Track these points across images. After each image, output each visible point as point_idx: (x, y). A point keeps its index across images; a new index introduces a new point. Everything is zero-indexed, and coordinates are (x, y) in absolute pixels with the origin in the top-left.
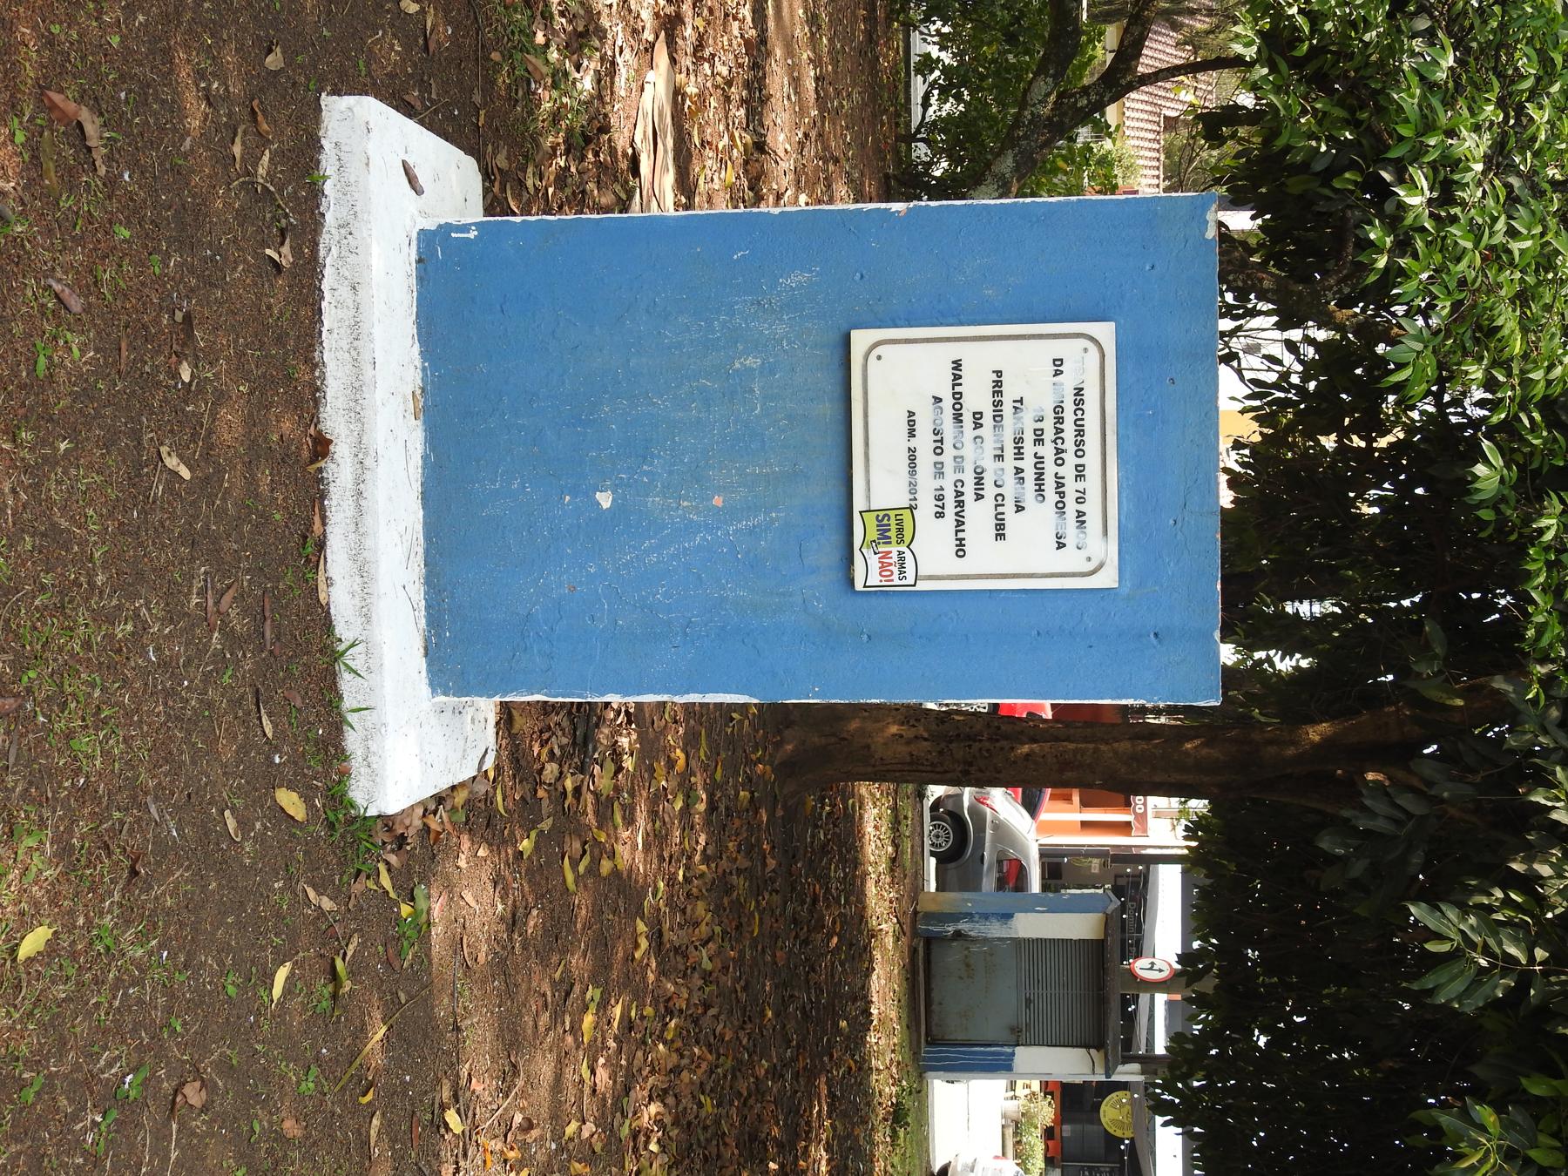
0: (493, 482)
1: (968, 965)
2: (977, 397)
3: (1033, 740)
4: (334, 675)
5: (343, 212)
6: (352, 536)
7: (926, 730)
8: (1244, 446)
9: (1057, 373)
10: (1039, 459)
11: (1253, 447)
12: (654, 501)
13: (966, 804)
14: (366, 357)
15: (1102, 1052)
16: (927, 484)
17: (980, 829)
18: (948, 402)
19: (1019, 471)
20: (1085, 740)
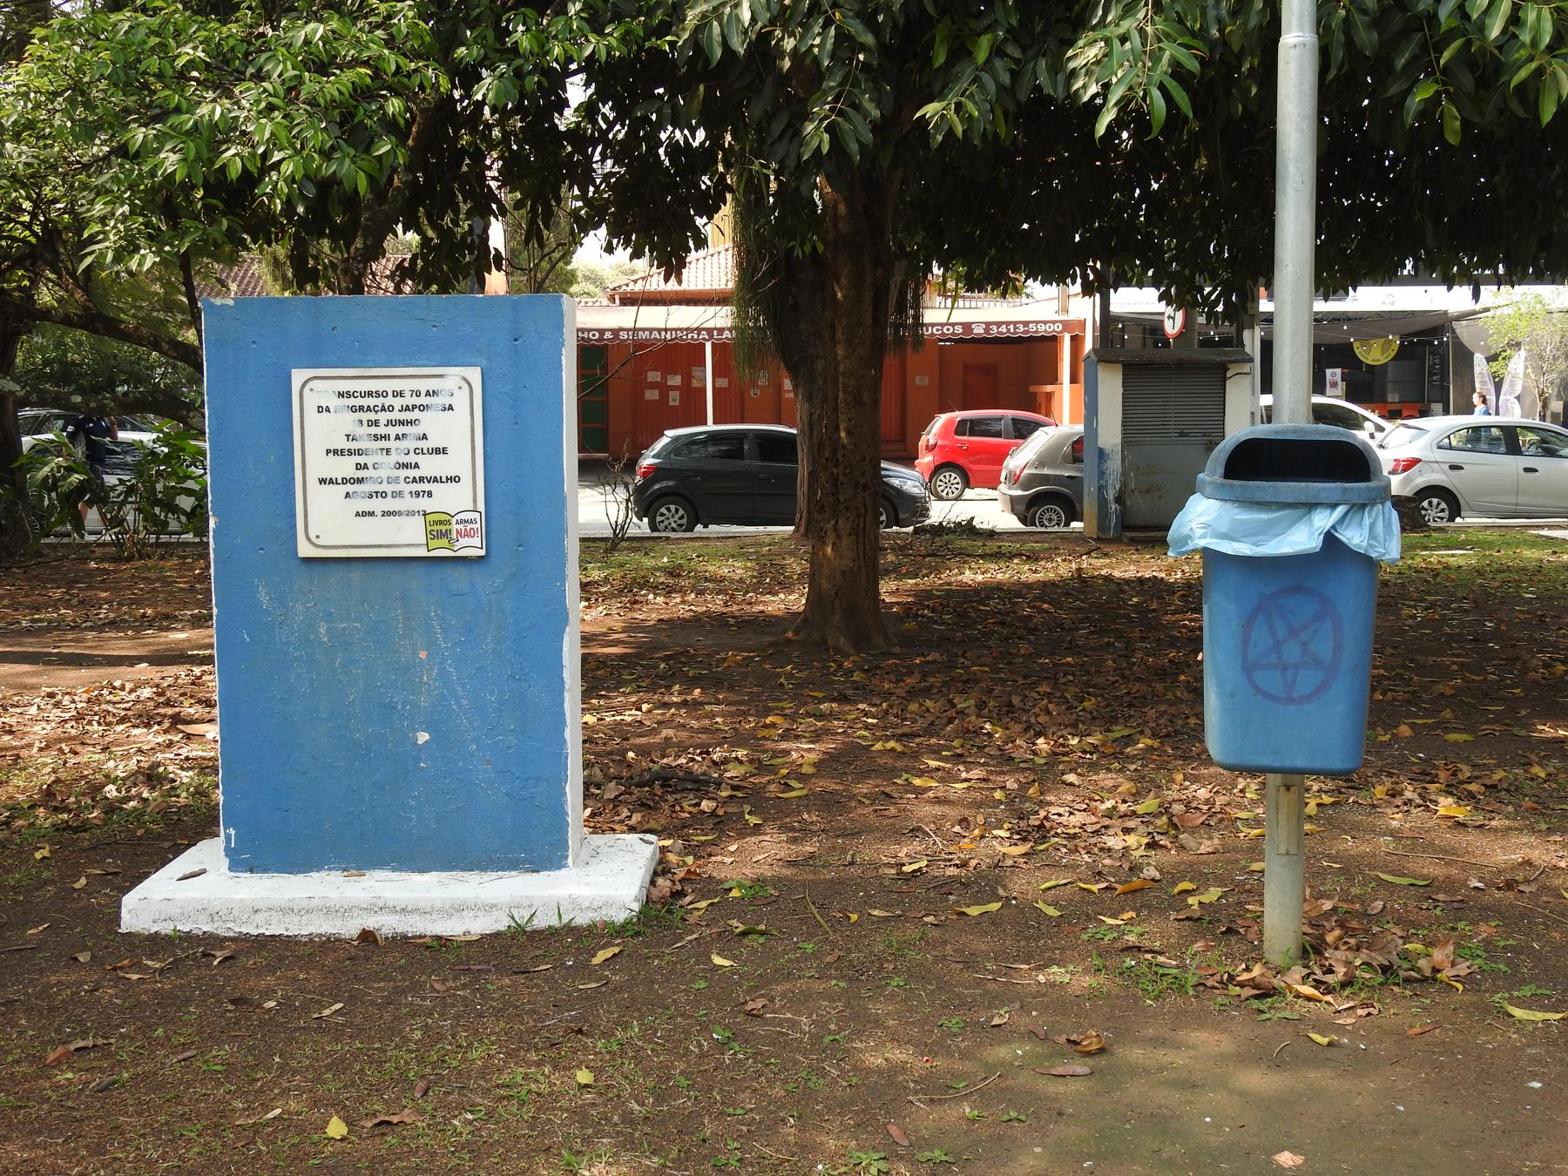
0: (410, 819)
1: (1148, 491)
2: (346, 467)
3: (837, 429)
4: (534, 931)
5: (203, 918)
6: (434, 917)
7: (828, 521)
8: (610, 244)
9: (328, 410)
10: (389, 423)
11: (612, 233)
12: (423, 701)
13: (1019, 493)
14: (305, 904)
15: (1229, 366)
16: (408, 503)
17: (1045, 479)
18: (349, 488)
19: (397, 438)
20: (836, 383)
